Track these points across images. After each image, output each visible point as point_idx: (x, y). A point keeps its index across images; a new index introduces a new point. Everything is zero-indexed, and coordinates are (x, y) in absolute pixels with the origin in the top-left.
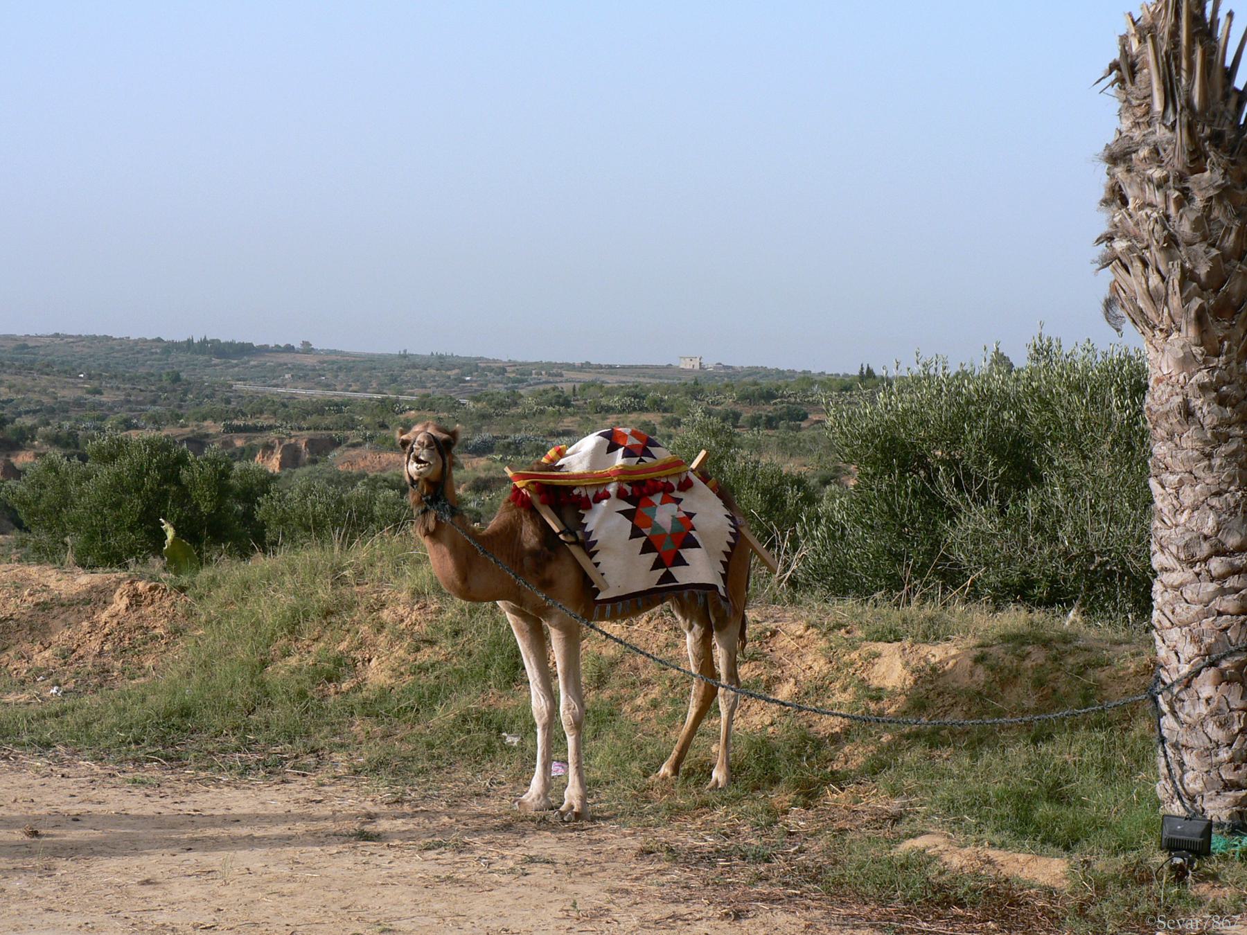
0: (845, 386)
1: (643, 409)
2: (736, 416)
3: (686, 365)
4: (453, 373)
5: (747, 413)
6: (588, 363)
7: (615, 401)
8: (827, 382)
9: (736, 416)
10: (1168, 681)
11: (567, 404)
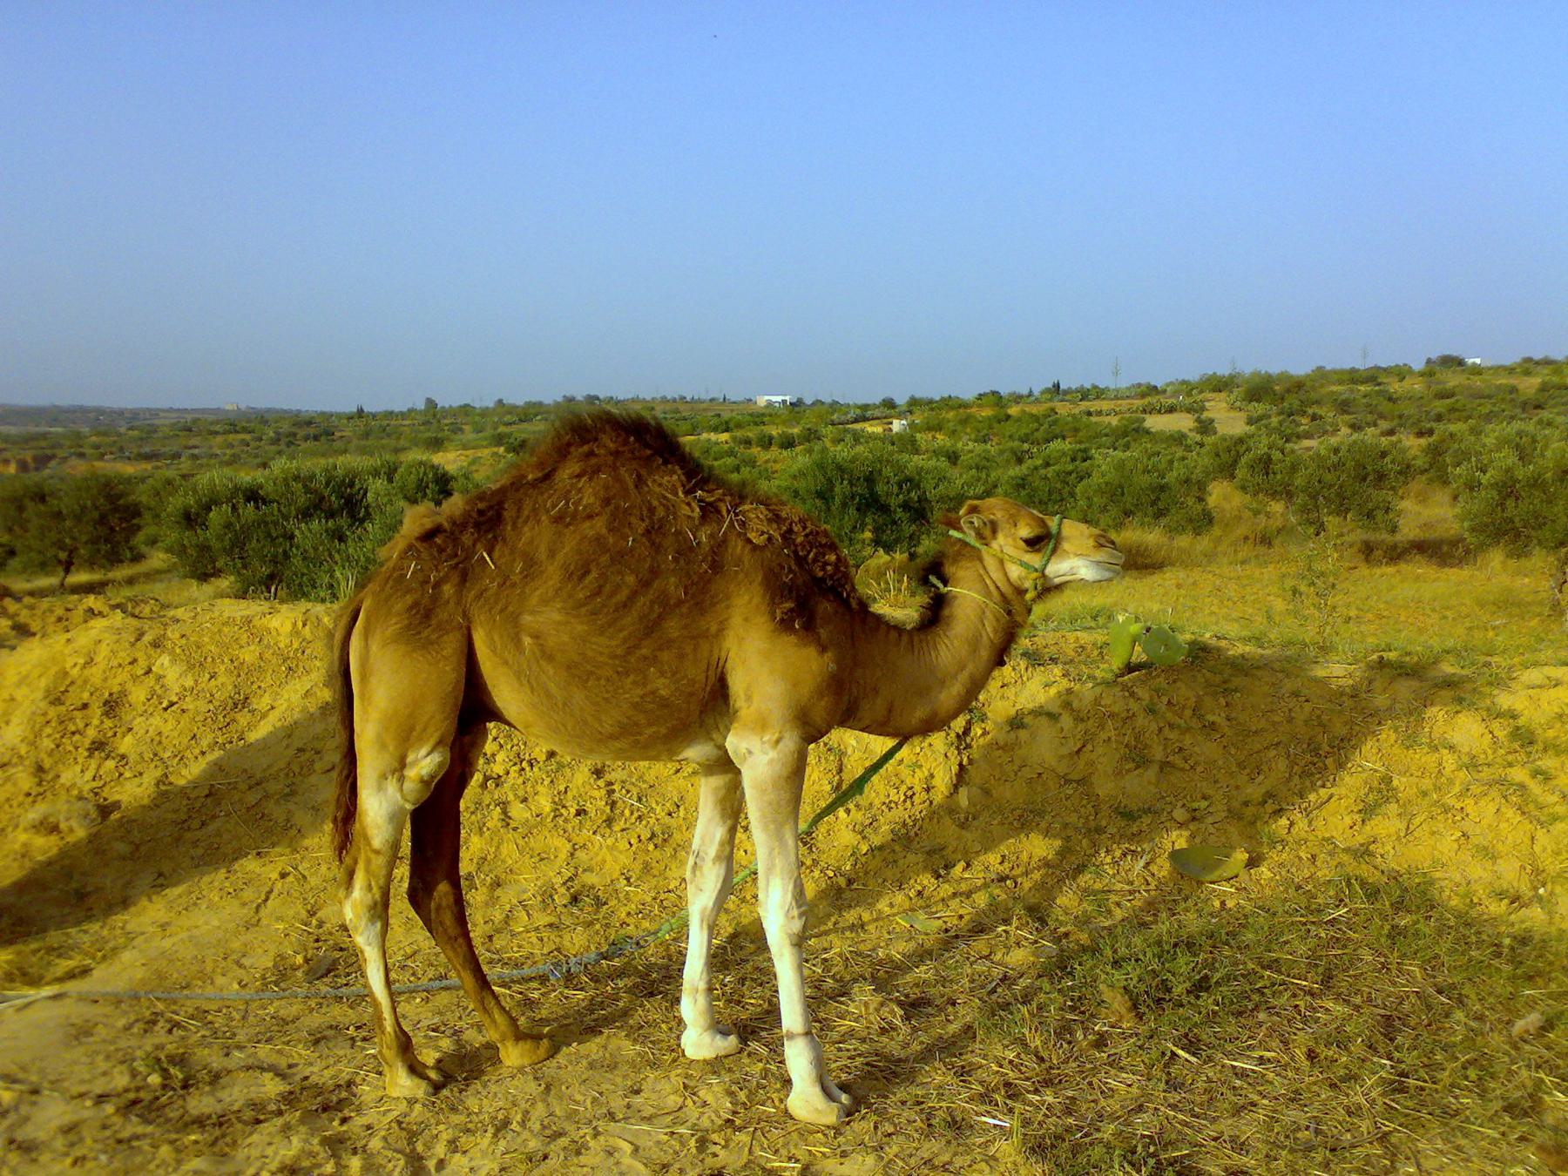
0: (350, 418)
1: (237, 432)
2: (295, 435)
3: (229, 407)
4: (92, 415)
5: (301, 433)
6: (1528, 360)
7: (217, 428)
8: (339, 416)
9: (295, 435)
10: (274, 535)
11: (190, 430)
